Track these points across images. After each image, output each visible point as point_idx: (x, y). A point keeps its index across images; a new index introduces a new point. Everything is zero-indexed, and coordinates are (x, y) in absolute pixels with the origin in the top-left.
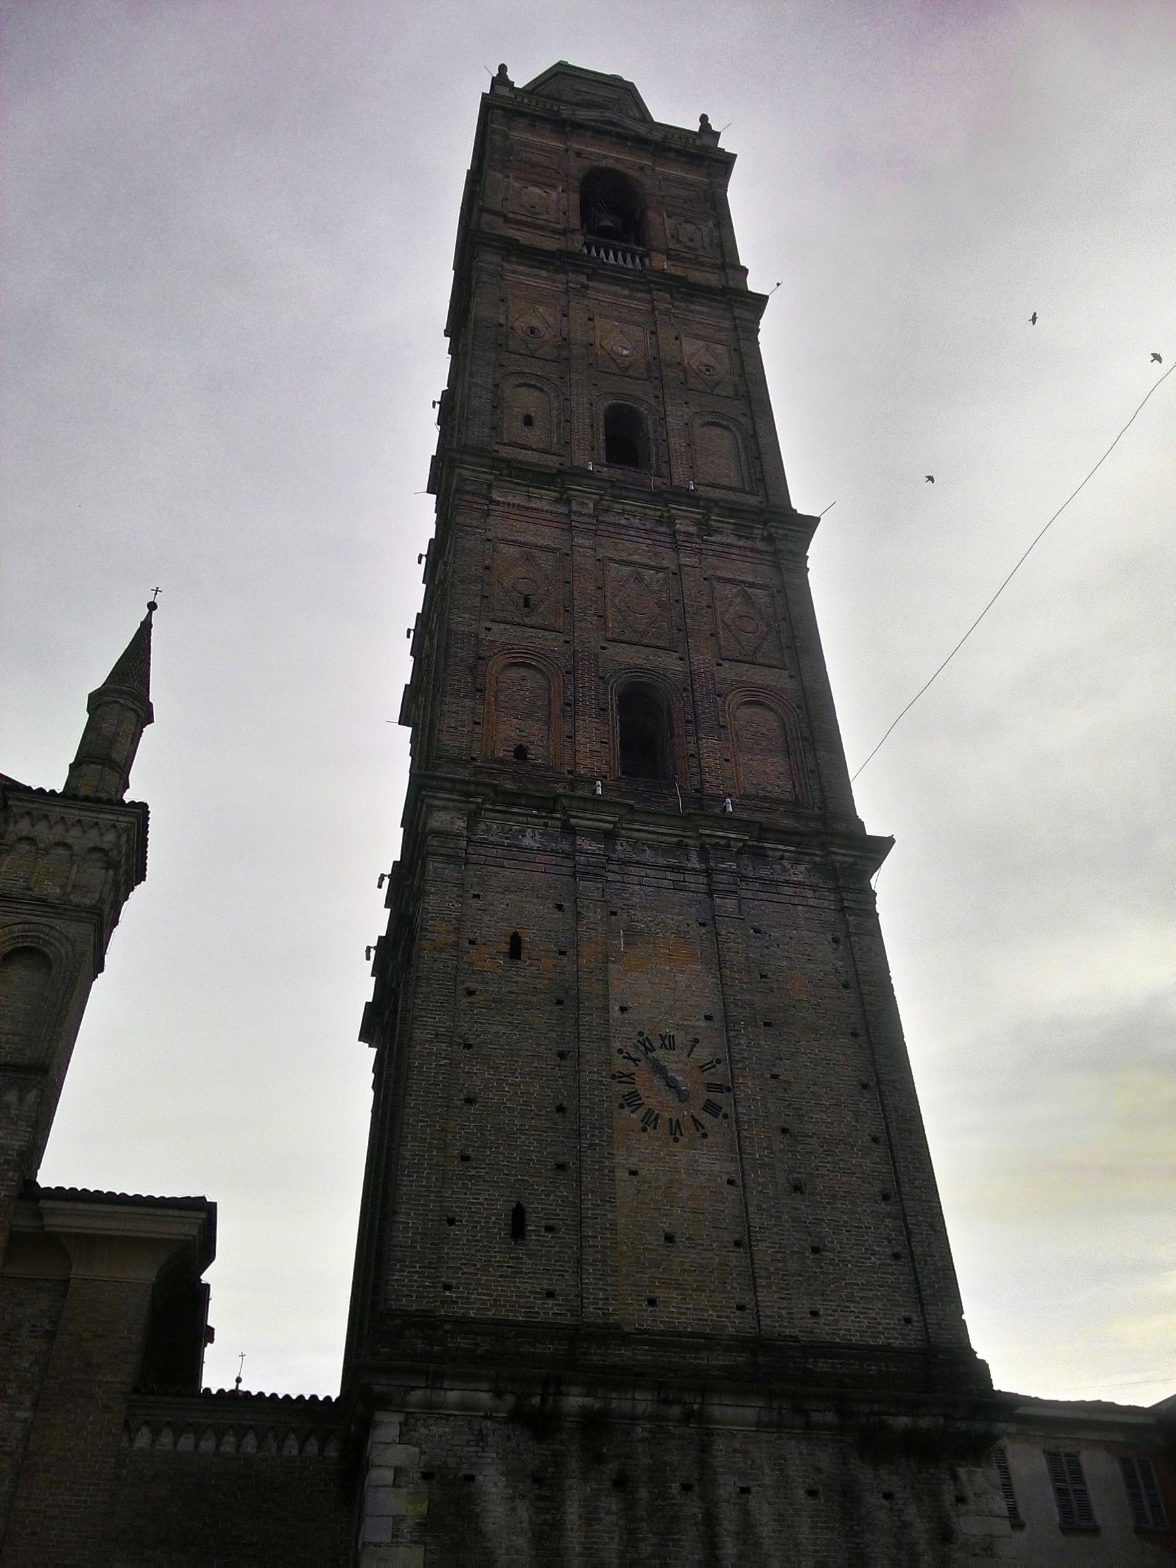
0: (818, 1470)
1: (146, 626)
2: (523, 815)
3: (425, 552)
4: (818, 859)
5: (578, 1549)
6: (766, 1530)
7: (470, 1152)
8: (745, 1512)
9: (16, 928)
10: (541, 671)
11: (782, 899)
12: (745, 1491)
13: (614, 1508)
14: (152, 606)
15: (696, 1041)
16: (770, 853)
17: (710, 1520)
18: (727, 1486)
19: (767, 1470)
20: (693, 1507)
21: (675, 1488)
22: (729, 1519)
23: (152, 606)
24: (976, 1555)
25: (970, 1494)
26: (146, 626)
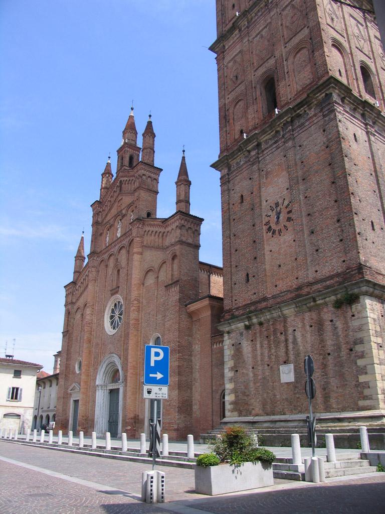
0: (312, 319)
1: (184, 158)
2: (238, 156)
3: (14, 358)
4: (315, 102)
5: (260, 354)
6: (299, 340)
7: (237, 264)
8: (294, 336)
9: (266, 425)
10: (303, 48)
11: (307, 127)
12: (295, 330)
13: (266, 343)
14: (184, 151)
15: (284, 199)
16: (301, 113)
17: (286, 340)
18: (290, 330)
19: (299, 323)
20: (282, 338)
21: (279, 334)
22: (290, 339)
23: (184, 151)
24: (356, 332)
25: (356, 313)
26: (184, 158)
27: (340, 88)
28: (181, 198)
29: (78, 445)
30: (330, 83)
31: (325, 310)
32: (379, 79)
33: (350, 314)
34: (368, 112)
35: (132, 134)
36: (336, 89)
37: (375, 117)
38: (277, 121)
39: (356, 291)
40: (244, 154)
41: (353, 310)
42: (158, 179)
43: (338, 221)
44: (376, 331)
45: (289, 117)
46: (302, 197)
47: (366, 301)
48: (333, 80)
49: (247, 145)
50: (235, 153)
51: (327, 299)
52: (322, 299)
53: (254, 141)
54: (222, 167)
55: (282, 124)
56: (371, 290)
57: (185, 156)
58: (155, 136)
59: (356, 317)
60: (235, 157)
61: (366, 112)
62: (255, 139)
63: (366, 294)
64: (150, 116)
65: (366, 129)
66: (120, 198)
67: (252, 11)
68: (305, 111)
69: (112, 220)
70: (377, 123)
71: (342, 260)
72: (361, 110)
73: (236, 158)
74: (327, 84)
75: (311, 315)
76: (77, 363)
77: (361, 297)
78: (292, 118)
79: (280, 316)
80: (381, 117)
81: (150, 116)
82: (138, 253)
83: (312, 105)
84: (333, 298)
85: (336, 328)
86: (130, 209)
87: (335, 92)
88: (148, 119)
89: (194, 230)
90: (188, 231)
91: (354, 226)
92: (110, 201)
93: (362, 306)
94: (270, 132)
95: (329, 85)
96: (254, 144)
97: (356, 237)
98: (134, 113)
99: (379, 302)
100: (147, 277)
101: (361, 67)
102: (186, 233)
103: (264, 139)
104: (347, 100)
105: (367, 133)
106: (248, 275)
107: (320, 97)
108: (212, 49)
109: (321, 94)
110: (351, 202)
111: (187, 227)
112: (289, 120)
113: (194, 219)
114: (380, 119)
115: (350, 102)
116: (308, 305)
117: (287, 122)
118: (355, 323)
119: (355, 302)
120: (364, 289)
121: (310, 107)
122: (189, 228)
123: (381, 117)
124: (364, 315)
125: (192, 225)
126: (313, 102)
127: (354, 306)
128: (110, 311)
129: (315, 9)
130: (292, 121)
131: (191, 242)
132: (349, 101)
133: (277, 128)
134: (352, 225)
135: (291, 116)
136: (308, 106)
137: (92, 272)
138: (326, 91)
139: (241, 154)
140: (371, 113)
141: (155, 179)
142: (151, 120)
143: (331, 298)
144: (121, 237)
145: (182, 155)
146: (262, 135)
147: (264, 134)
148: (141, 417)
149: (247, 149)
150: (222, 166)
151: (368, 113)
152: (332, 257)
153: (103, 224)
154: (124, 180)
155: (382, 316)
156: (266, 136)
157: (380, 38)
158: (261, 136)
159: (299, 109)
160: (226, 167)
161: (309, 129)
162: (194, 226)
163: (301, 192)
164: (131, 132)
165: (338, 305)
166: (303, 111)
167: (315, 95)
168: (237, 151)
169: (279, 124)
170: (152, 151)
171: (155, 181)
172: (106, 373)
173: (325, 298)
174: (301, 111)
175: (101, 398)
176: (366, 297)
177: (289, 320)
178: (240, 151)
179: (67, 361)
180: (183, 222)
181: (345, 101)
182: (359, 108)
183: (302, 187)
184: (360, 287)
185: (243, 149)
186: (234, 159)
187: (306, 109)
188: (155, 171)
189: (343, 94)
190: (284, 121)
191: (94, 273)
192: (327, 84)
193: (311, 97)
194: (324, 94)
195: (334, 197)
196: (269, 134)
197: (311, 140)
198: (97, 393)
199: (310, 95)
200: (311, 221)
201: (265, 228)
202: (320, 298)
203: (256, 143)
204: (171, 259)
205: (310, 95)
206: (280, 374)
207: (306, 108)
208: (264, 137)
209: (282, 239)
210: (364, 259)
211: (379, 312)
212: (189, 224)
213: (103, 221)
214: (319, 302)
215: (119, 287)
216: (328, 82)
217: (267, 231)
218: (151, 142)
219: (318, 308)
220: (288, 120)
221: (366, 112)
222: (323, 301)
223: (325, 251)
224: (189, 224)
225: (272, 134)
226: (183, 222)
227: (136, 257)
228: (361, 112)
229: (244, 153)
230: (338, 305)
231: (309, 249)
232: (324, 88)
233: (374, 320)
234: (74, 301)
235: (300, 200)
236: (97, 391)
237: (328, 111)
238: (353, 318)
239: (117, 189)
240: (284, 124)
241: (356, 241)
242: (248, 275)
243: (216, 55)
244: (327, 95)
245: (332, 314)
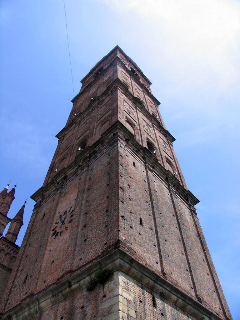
1: (24, 206)
4: (107, 141)
14: (26, 202)
16: (96, 150)
23: (26, 202)
26: (24, 206)
27: (124, 131)
28: (11, 231)
30: (117, 126)
31: (79, 296)
32: (160, 152)
33: (102, 294)
34: (147, 156)
35: (1, 199)
36: (121, 131)
37: (153, 162)
38: (79, 157)
39: (110, 266)
40: (55, 186)
41: (106, 289)
42: (6, 225)
43: (107, 211)
44: (128, 315)
45: (88, 153)
46: (84, 202)
47: (119, 277)
48: (119, 124)
49: (57, 177)
50: (49, 185)
51: (82, 282)
52: (77, 282)
53: (63, 174)
54: (38, 198)
55: (83, 159)
56: (127, 266)
57: (25, 205)
58: (14, 198)
59: (107, 297)
60: (49, 188)
61: (146, 156)
62: (63, 173)
63: (120, 269)
64: (15, 186)
65: (145, 166)
67: (84, 113)
68: (100, 148)
70: (155, 168)
71: (104, 243)
72: (142, 154)
73: (49, 190)
74: (114, 126)
75: (65, 305)
77: (115, 273)
78: (90, 154)
79: (37, 312)
80: (158, 164)
81: (15, 186)
83: (104, 143)
84: (88, 279)
85: (85, 315)
87: (120, 132)
88: (13, 187)
89: (12, 256)
90: (6, 255)
91: (118, 209)
93: (114, 283)
94: (74, 166)
95: (115, 127)
96: (62, 177)
97: (118, 218)
98: (8, 188)
99: (138, 286)
101: (147, 141)
102: (4, 256)
103: (70, 173)
104: (130, 142)
105: (146, 168)
106: (27, 275)
107: (110, 136)
108: (57, 136)
109: (110, 134)
110: (118, 192)
111: (7, 252)
112: (88, 155)
113: (14, 247)
114: (158, 166)
115: (133, 145)
116: (64, 292)
117: (87, 157)
118: (105, 305)
119: (108, 280)
120: (118, 262)
121: (103, 144)
122: (8, 253)
123: (158, 164)
124: (115, 293)
125: (12, 252)
126: (105, 141)
127: (106, 285)
129: (117, 100)
130: (90, 157)
131: (6, 265)
132: (132, 144)
133: (80, 163)
134: (117, 210)
135: (90, 153)
136: (101, 144)
138: (114, 131)
139: (52, 186)
140: (150, 158)
141: (3, 225)
142: (16, 188)
143: (85, 279)
145: (24, 204)
146: (69, 170)
147: (70, 169)
149: (57, 181)
150: (38, 197)
151: (148, 158)
152: (97, 243)
155: (141, 301)
156: (72, 170)
158: (68, 171)
159: (95, 147)
160: (41, 197)
161: (100, 157)
162: (13, 253)
163: (84, 199)
164: (2, 197)
165: (92, 287)
166: (98, 149)
167: (106, 135)
168: (50, 184)
169: (81, 160)
170: (8, 206)
171: (3, 226)
173: (80, 281)
174: (97, 149)
176: (120, 273)
177: (44, 314)
178: (52, 184)
180: (4, 246)
181: (129, 142)
182: (140, 152)
183: (85, 195)
184: (114, 261)
185: (54, 182)
186: (48, 191)
187: (100, 147)
188: (5, 219)
189: (127, 136)
190: (84, 156)
192: (114, 126)
193: (104, 137)
194: (113, 134)
195: (107, 195)
196: (73, 169)
197: (100, 164)
199: (103, 136)
200: (86, 218)
201: (52, 233)
202: (76, 281)
203: (64, 175)
205: (103, 136)
207: (100, 146)
208: (70, 171)
209: (61, 238)
210: (124, 238)
211: (137, 295)
212: (9, 250)
214: (74, 286)
216: (115, 125)
217: (53, 235)
218: (10, 200)
219: (73, 293)
220: (87, 156)
221: (146, 156)
222: (78, 284)
223: (91, 239)
224: (9, 250)
225: (75, 168)
226: (4, 246)
228: (142, 155)
229: (55, 185)
230: (92, 287)
231: (80, 240)
232: (113, 129)
233: (128, 301)
235: (81, 204)
237: (114, 142)
238: (104, 299)
240: (84, 159)
241: (118, 222)
242: (27, 275)
243: (58, 140)
244: (114, 134)
245: (85, 299)
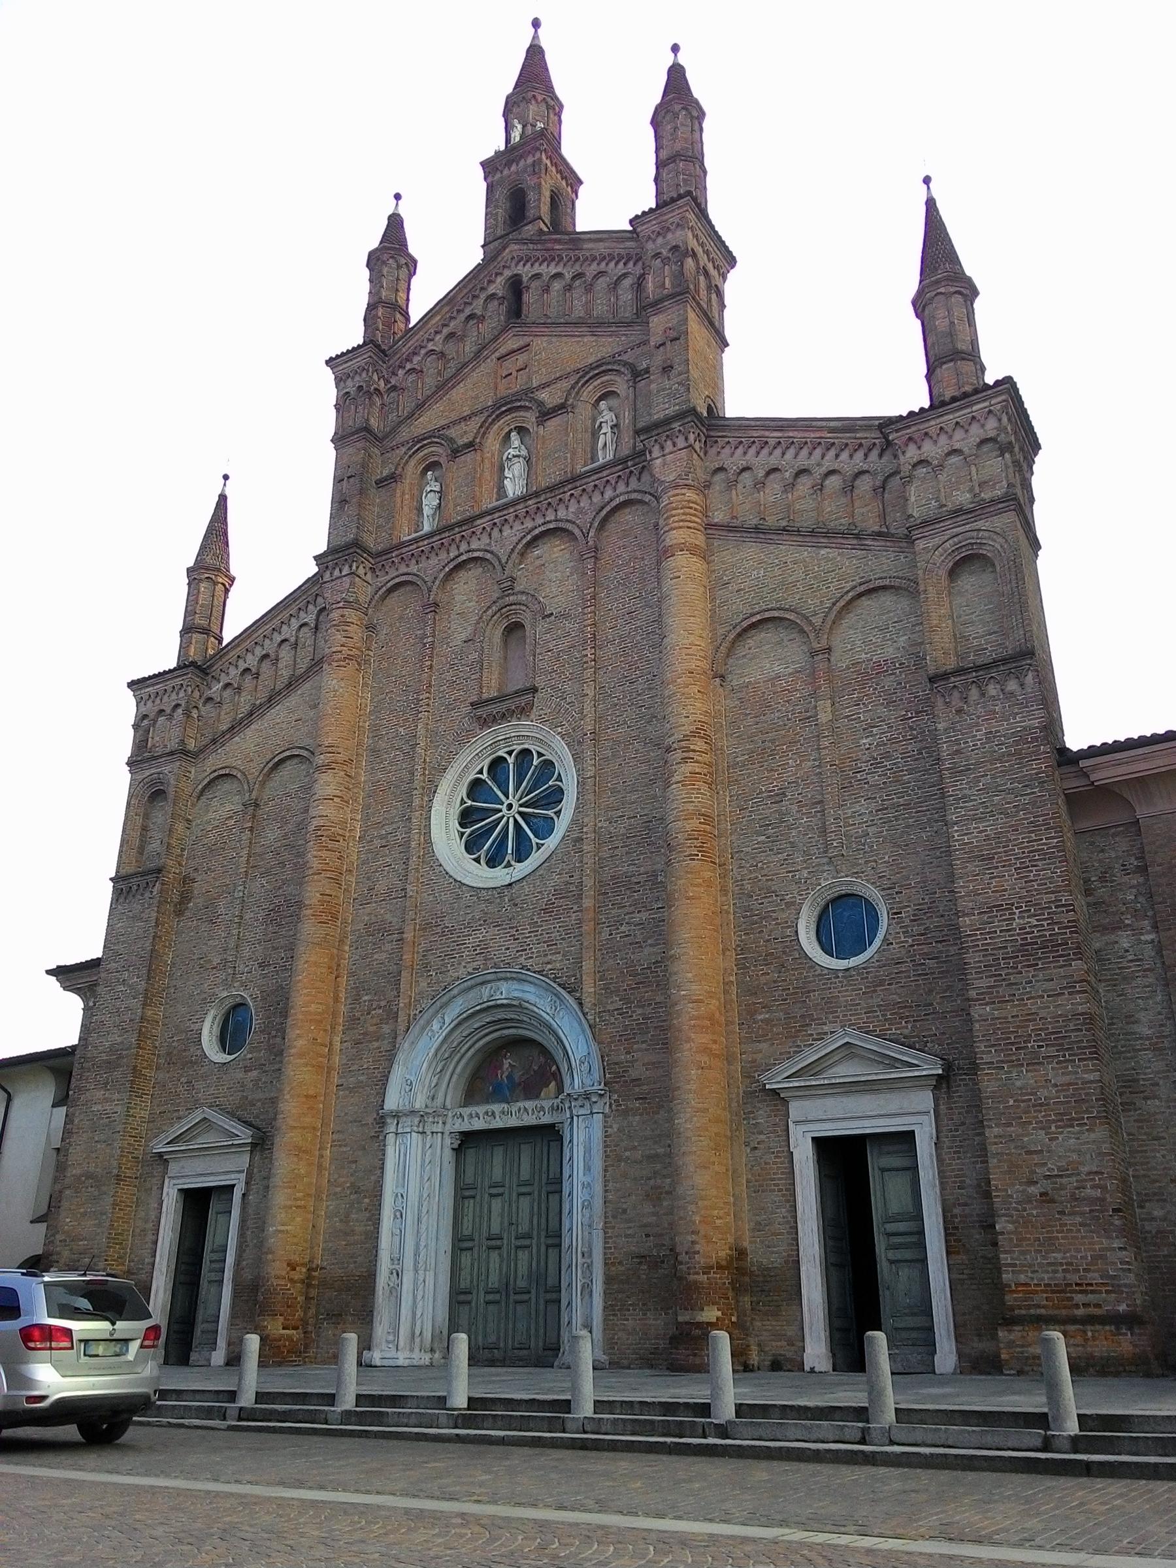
26: (931, 204)
29: (232, 1396)
66: (513, 344)
69: (479, 420)
76: (212, 1013)
82: (693, 550)
86: (412, 462)
92: (442, 355)
100: (741, 651)
128: (463, 792)
137: (347, 623)
144: (523, 499)
148: (149, 1412)
153: (388, 443)
154: (537, 276)
157: (240, 614)
172: (445, 1055)
175: (415, 1181)
179: (145, 1005)
191: (356, 632)
198: (390, 1151)
204: (943, 573)
206: (953, 1305)
213: (394, 430)
215: (534, 690)
227: (685, 565)
234: (191, 745)
236: (391, 1138)
239: (485, 308)
243: (502, 148)
